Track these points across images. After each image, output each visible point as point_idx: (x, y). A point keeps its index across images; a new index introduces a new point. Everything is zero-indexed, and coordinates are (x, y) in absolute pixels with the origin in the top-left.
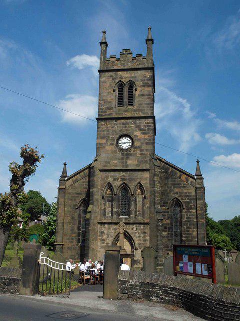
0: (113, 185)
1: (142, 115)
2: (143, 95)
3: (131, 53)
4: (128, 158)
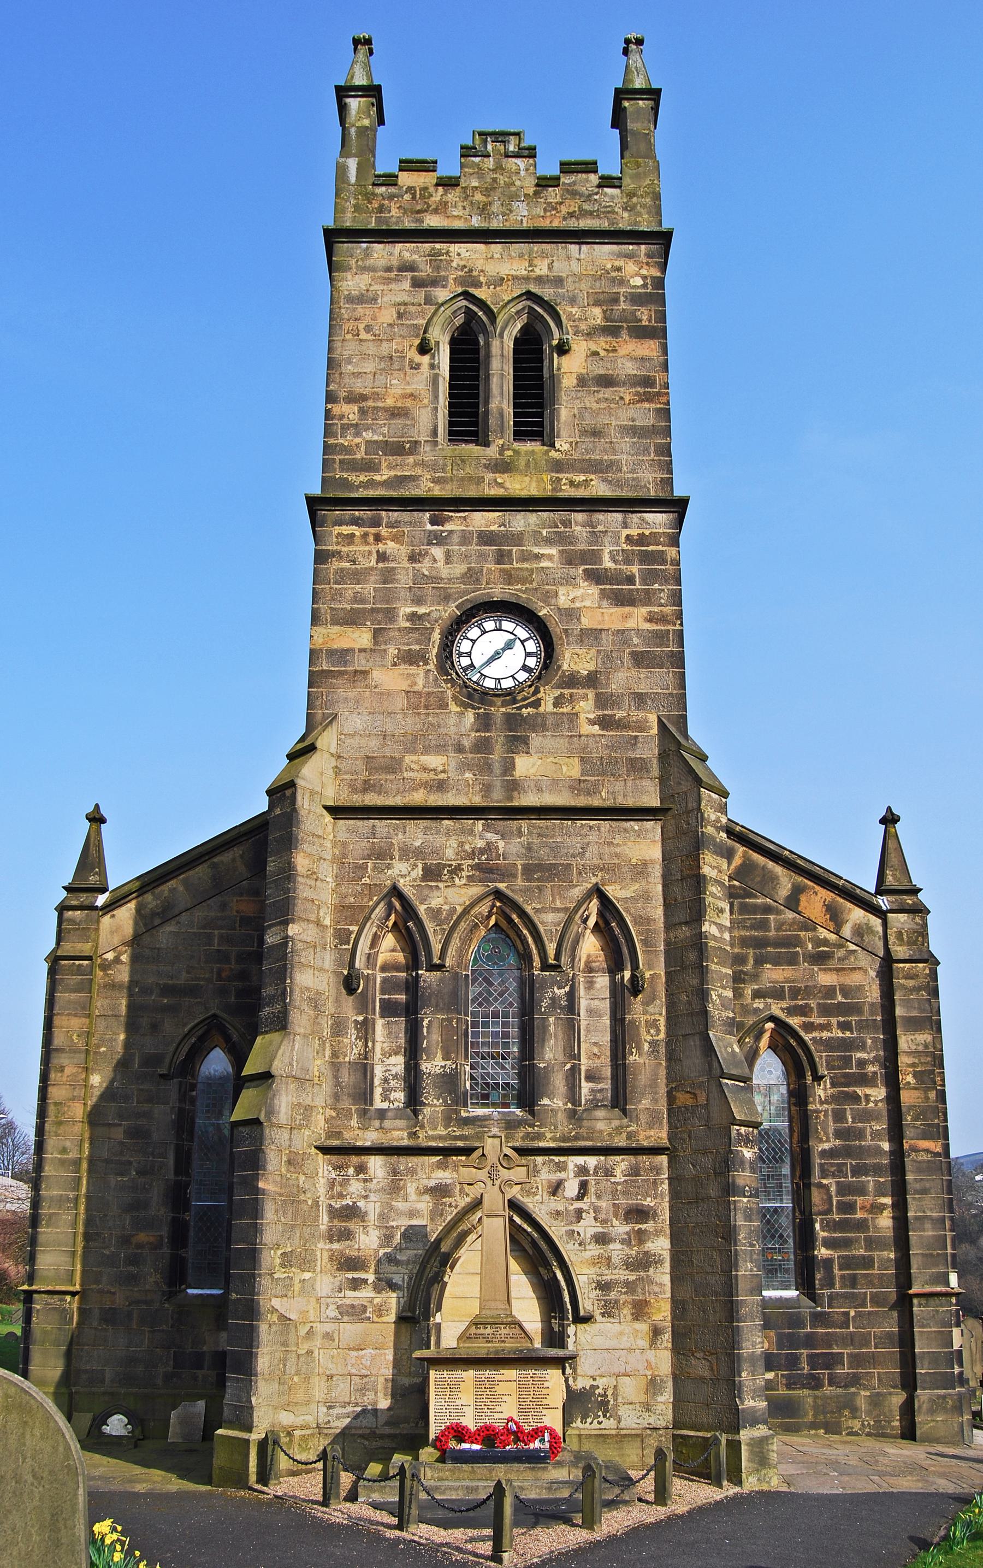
0: (422, 909)
1: (599, 489)
2: (606, 381)
3: (530, 153)
4: (518, 743)
